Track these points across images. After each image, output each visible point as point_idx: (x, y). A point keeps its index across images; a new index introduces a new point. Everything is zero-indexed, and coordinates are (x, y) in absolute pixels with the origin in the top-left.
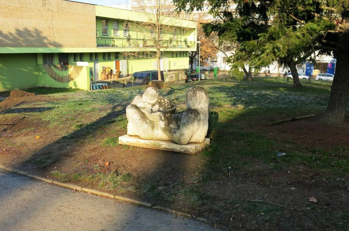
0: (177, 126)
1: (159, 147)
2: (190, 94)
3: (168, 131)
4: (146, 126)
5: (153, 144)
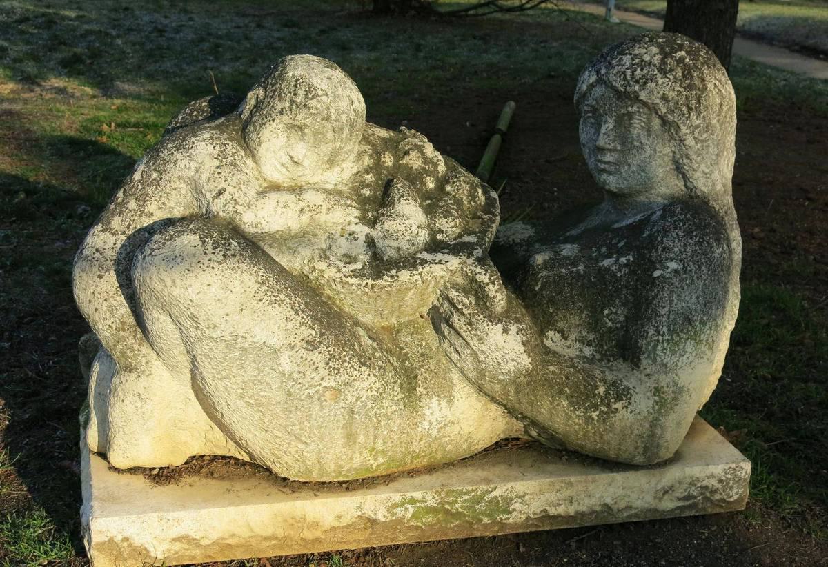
0: (591, 337)
1: (495, 522)
2: (664, 98)
3: (561, 392)
4: (366, 383)
5: (433, 510)
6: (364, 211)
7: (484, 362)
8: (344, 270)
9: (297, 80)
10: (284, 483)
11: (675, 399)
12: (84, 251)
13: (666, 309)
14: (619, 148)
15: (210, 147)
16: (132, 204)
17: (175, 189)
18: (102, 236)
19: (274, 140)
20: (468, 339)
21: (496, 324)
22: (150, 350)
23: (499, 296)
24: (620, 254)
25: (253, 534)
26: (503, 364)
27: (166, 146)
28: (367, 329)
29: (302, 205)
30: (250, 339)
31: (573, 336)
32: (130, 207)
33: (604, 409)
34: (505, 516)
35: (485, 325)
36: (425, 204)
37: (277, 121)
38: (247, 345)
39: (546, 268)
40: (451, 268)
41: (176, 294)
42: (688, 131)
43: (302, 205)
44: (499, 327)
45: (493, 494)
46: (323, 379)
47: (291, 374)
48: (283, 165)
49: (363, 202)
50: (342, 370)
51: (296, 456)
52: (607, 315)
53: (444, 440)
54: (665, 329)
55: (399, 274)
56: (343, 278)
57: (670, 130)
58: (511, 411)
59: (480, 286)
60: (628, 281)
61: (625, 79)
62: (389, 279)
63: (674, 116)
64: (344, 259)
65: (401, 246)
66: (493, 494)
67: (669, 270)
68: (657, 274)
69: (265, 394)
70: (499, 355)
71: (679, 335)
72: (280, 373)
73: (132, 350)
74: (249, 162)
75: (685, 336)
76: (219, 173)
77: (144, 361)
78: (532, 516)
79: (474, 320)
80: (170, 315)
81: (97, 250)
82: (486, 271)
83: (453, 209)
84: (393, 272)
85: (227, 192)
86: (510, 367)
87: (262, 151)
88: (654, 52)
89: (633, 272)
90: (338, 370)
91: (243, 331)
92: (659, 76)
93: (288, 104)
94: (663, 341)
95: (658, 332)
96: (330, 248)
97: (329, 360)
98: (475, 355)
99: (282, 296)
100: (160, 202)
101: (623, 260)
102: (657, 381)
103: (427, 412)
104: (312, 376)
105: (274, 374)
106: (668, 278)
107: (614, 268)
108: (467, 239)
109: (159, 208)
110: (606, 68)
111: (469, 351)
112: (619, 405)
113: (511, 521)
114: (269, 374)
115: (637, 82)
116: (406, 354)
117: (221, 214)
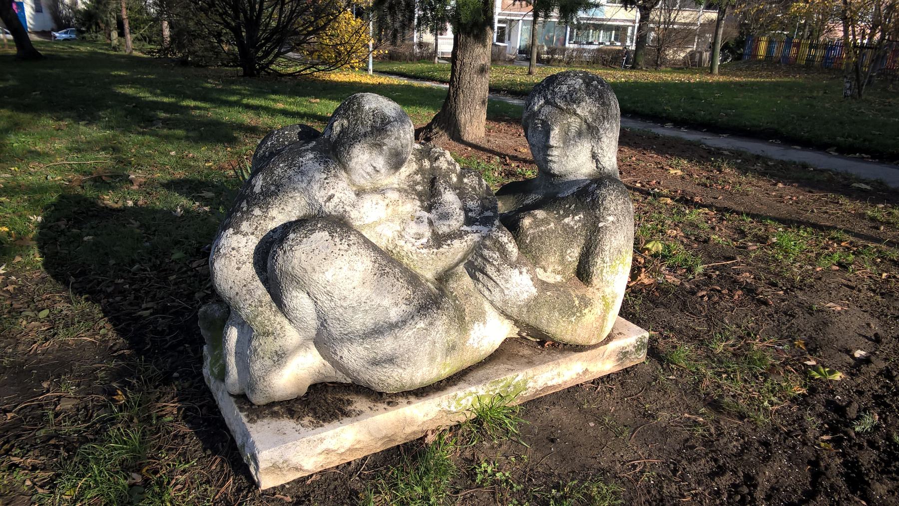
0: (560, 268)
6: (422, 201)
8: (416, 244)
11: (613, 302)
12: (221, 251)
13: (608, 247)
17: (291, 198)
18: (235, 237)
19: (361, 156)
20: (498, 282)
22: (283, 319)
24: (574, 215)
27: (278, 165)
29: (387, 201)
31: (549, 270)
32: (255, 214)
33: (578, 314)
34: (525, 392)
37: (362, 141)
38: (367, 308)
39: (531, 228)
43: (387, 201)
44: (517, 271)
45: (517, 380)
48: (368, 173)
53: (481, 349)
55: (453, 242)
57: (592, 132)
58: (516, 322)
59: (501, 245)
60: (581, 231)
62: (447, 247)
66: (517, 380)
68: (601, 225)
73: (269, 320)
74: (343, 173)
76: (327, 183)
77: (279, 327)
79: (501, 268)
80: (308, 293)
81: (233, 249)
84: (449, 242)
85: (336, 197)
86: (525, 296)
87: (352, 164)
89: (584, 225)
91: (365, 298)
92: (587, 98)
96: (404, 229)
101: (577, 218)
102: (603, 292)
107: (572, 223)
110: (551, 94)
111: (498, 289)
112: (586, 311)
116: (456, 296)
117: (333, 213)
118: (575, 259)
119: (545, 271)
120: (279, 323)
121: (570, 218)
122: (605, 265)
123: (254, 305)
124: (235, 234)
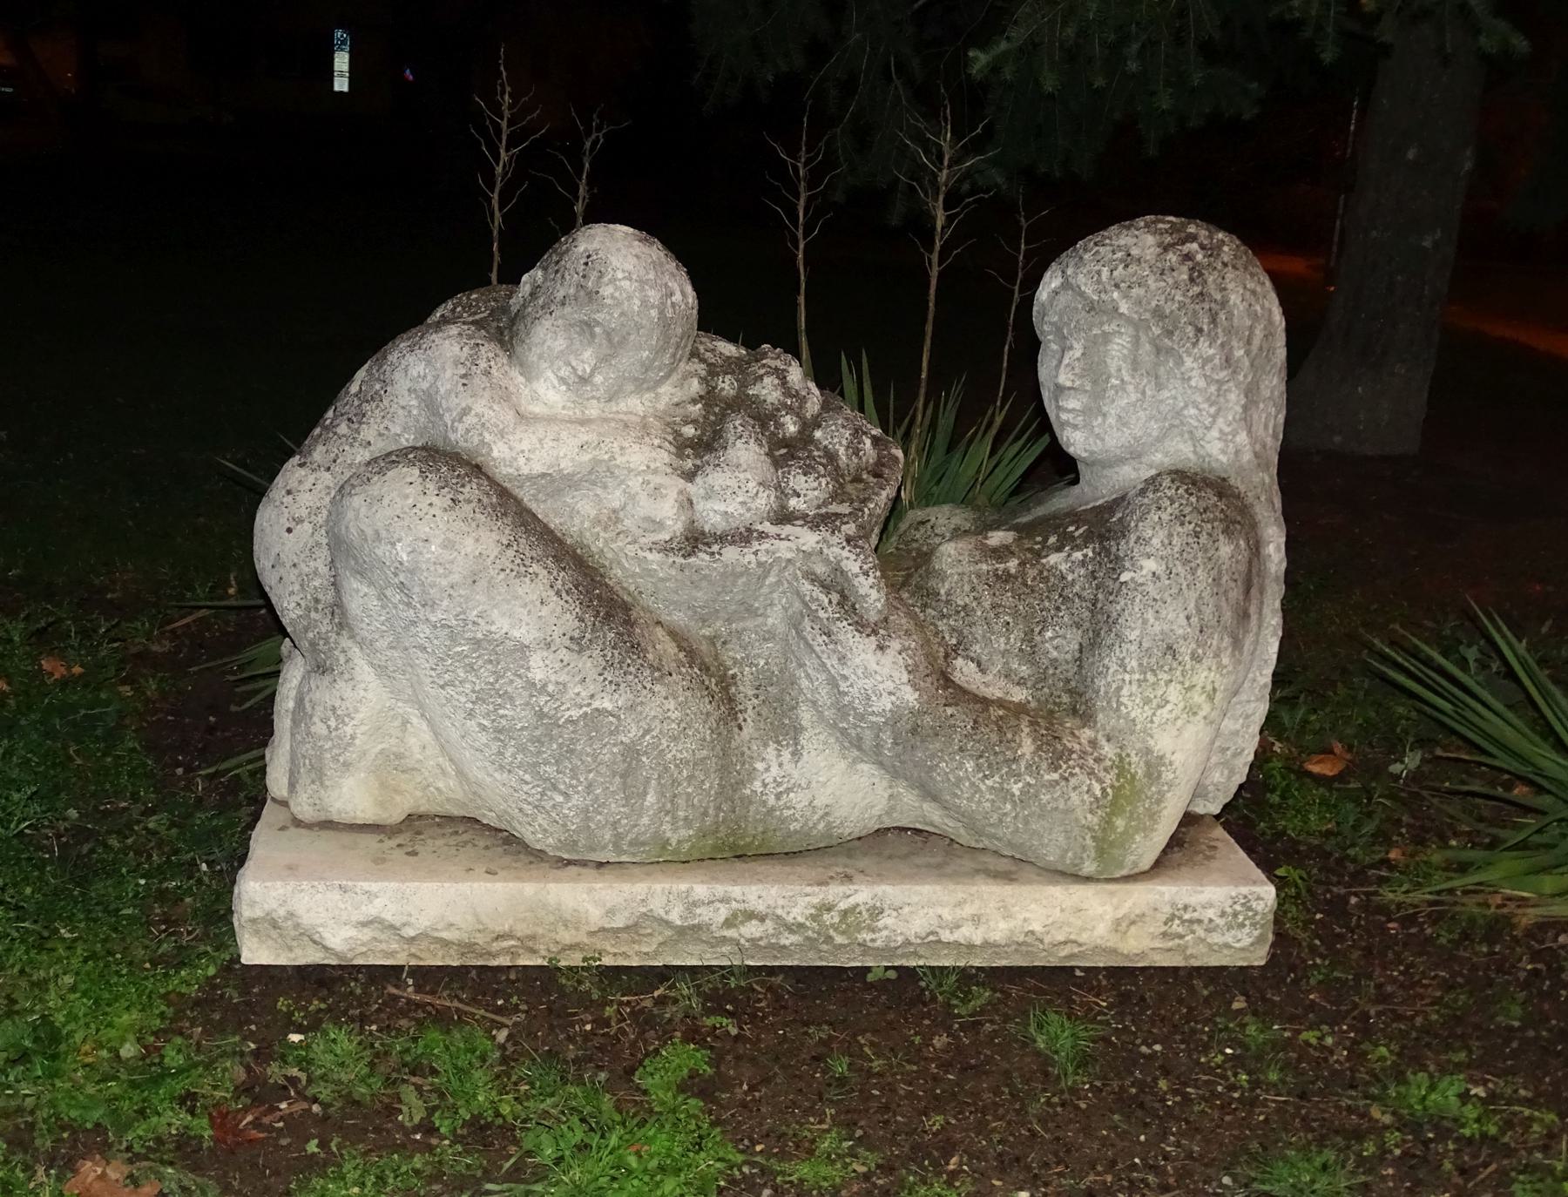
7: (846, 694)
9: (589, 257)
10: (538, 856)
14: (1088, 388)
15: (457, 349)
16: (343, 429)
21: (868, 635)
23: (874, 594)
25: (481, 927)
26: (874, 698)
28: (673, 634)
30: (484, 627)
35: (850, 636)
36: (777, 453)
38: (479, 636)
40: (804, 548)
41: (379, 552)
42: (1195, 365)
46: (592, 696)
47: (545, 685)
49: (682, 446)
50: (623, 685)
51: (554, 815)
52: (1051, 639)
54: (1134, 663)
56: (639, 552)
61: (1099, 282)
62: (707, 558)
63: (1173, 341)
64: (645, 525)
65: (730, 510)
67: (1144, 572)
68: (1125, 577)
69: (506, 712)
70: (868, 684)
71: (1156, 675)
72: (528, 681)
75: (1166, 677)
78: (913, 939)
82: (857, 555)
83: (821, 464)
84: (715, 548)
88: (1148, 244)
90: (618, 685)
91: (475, 613)
93: (572, 291)
94: (1130, 682)
95: (1123, 665)
97: (605, 669)
98: (833, 682)
99: (535, 568)
100: (382, 426)
101: (1078, 555)
103: (760, 766)
104: (576, 691)
105: (519, 682)
106: (1142, 585)
107: (1063, 567)
108: (834, 508)
109: (380, 435)
113: (878, 943)
114: (512, 681)
115: (1117, 286)
118: (1069, 657)
119: (983, 671)
120: (344, 651)
121: (1064, 554)
122: (1127, 677)
123: (303, 605)
124: (301, 465)
